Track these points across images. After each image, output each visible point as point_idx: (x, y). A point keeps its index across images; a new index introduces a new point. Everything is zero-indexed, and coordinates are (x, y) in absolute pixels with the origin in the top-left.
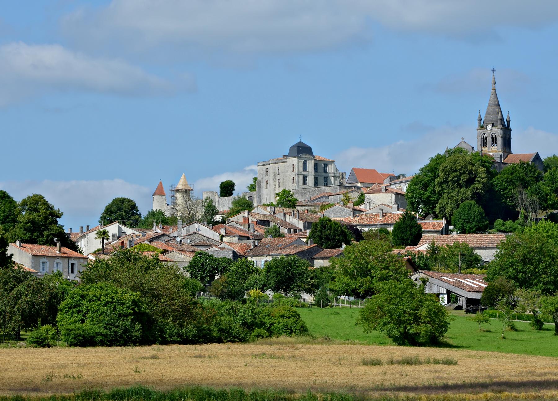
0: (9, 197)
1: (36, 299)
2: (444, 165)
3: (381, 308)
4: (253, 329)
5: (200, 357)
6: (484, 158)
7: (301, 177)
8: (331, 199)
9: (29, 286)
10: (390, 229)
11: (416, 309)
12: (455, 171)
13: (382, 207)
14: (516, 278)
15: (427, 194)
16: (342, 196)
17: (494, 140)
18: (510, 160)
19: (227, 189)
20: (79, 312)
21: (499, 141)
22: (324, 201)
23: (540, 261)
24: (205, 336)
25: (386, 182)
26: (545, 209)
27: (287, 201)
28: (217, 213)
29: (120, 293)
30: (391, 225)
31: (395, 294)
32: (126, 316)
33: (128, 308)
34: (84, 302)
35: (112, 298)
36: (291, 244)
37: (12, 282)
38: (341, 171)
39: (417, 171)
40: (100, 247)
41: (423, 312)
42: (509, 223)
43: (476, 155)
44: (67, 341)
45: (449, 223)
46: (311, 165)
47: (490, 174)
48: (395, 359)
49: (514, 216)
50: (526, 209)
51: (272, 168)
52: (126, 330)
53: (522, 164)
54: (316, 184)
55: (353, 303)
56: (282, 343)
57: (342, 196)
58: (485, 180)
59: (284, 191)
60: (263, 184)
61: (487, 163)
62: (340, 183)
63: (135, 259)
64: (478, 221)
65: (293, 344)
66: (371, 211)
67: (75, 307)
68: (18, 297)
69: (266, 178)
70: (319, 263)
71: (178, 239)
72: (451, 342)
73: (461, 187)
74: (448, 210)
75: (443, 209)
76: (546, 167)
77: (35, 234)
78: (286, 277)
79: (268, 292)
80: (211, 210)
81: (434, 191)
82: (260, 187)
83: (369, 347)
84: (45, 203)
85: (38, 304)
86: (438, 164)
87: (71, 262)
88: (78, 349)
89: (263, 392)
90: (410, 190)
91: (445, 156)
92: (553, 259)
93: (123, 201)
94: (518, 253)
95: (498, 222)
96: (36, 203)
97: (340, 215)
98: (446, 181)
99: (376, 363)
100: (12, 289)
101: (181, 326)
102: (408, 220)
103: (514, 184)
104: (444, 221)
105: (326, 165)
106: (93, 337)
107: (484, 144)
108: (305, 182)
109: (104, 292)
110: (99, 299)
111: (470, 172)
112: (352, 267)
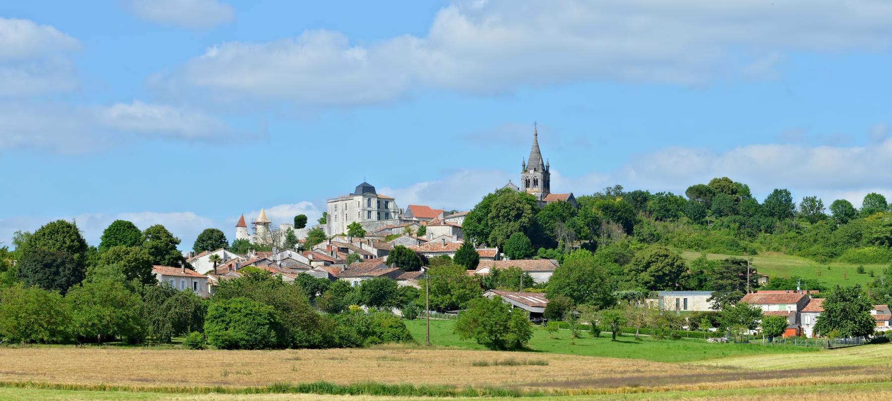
0: (134, 227)
1: (183, 310)
2: (496, 202)
3: (475, 321)
4: (365, 337)
5: (333, 359)
6: (530, 198)
7: (366, 213)
8: (394, 231)
9: (177, 300)
10: (452, 256)
11: (506, 321)
12: (505, 208)
13: (442, 238)
14: (572, 296)
15: (481, 227)
16: (403, 229)
17: (536, 182)
18: (549, 200)
19: (300, 222)
20: (223, 321)
21: (540, 183)
22: (389, 233)
23: (592, 282)
24: (328, 342)
25: (441, 217)
26: (579, 239)
27: (356, 231)
28: (297, 242)
29: (257, 307)
30: (451, 252)
31: (488, 309)
32: (264, 325)
33: (265, 318)
34: (227, 313)
35: (251, 310)
36: (376, 268)
37: (162, 297)
38: (400, 207)
39: (473, 208)
40: (212, 268)
41: (512, 323)
42: (550, 251)
43: (522, 195)
44: (216, 345)
45: (501, 251)
46: (374, 202)
47: (535, 211)
48: (499, 361)
49: (555, 246)
50: (564, 240)
51: (340, 204)
52: (264, 337)
53: (560, 202)
54: (379, 218)
55: (436, 316)
56: (393, 349)
57: (403, 229)
58: (530, 216)
59: (354, 223)
60: (333, 218)
61: (531, 201)
62: (400, 218)
63: (263, 279)
64: (526, 249)
65: (403, 350)
66: (434, 241)
67: (219, 317)
68: (169, 308)
69: (336, 213)
70: (402, 284)
71: (278, 263)
72: (532, 347)
73: (510, 221)
74: (499, 240)
75: (494, 239)
76: (579, 206)
77: (158, 258)
78: (379, 295)
79: (363, 307)
80: (291, 240)
81: (487, 224)
82: (330, 220)
83: (468, 351)
84: (166, 232)
85: (185, 315)
86: (491, 202)
87: (194, 281)
88: (226, 351)
89: (430, 387)
90: (466, 223)
91: (495, 195)
92: (602, 280)
93: (212, 231)
94: (574, 275)
95: (541, 250)
96: (158, 232)
97: (410, 244)
98: (498, 216)
99: (484, 364)
100: (163, 302)
101: (309, 334)
102: (467, 247)
103: (554, 219)
104: (497, 249)
105: (387, 203)
106: (237, 342)
107: (527, 185)
108: (369, 217)
109: (244, 306)
110: (240, 311)
111: (518, 209)
112: (434, 287)
